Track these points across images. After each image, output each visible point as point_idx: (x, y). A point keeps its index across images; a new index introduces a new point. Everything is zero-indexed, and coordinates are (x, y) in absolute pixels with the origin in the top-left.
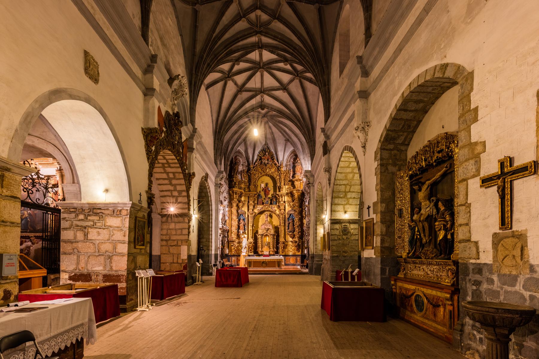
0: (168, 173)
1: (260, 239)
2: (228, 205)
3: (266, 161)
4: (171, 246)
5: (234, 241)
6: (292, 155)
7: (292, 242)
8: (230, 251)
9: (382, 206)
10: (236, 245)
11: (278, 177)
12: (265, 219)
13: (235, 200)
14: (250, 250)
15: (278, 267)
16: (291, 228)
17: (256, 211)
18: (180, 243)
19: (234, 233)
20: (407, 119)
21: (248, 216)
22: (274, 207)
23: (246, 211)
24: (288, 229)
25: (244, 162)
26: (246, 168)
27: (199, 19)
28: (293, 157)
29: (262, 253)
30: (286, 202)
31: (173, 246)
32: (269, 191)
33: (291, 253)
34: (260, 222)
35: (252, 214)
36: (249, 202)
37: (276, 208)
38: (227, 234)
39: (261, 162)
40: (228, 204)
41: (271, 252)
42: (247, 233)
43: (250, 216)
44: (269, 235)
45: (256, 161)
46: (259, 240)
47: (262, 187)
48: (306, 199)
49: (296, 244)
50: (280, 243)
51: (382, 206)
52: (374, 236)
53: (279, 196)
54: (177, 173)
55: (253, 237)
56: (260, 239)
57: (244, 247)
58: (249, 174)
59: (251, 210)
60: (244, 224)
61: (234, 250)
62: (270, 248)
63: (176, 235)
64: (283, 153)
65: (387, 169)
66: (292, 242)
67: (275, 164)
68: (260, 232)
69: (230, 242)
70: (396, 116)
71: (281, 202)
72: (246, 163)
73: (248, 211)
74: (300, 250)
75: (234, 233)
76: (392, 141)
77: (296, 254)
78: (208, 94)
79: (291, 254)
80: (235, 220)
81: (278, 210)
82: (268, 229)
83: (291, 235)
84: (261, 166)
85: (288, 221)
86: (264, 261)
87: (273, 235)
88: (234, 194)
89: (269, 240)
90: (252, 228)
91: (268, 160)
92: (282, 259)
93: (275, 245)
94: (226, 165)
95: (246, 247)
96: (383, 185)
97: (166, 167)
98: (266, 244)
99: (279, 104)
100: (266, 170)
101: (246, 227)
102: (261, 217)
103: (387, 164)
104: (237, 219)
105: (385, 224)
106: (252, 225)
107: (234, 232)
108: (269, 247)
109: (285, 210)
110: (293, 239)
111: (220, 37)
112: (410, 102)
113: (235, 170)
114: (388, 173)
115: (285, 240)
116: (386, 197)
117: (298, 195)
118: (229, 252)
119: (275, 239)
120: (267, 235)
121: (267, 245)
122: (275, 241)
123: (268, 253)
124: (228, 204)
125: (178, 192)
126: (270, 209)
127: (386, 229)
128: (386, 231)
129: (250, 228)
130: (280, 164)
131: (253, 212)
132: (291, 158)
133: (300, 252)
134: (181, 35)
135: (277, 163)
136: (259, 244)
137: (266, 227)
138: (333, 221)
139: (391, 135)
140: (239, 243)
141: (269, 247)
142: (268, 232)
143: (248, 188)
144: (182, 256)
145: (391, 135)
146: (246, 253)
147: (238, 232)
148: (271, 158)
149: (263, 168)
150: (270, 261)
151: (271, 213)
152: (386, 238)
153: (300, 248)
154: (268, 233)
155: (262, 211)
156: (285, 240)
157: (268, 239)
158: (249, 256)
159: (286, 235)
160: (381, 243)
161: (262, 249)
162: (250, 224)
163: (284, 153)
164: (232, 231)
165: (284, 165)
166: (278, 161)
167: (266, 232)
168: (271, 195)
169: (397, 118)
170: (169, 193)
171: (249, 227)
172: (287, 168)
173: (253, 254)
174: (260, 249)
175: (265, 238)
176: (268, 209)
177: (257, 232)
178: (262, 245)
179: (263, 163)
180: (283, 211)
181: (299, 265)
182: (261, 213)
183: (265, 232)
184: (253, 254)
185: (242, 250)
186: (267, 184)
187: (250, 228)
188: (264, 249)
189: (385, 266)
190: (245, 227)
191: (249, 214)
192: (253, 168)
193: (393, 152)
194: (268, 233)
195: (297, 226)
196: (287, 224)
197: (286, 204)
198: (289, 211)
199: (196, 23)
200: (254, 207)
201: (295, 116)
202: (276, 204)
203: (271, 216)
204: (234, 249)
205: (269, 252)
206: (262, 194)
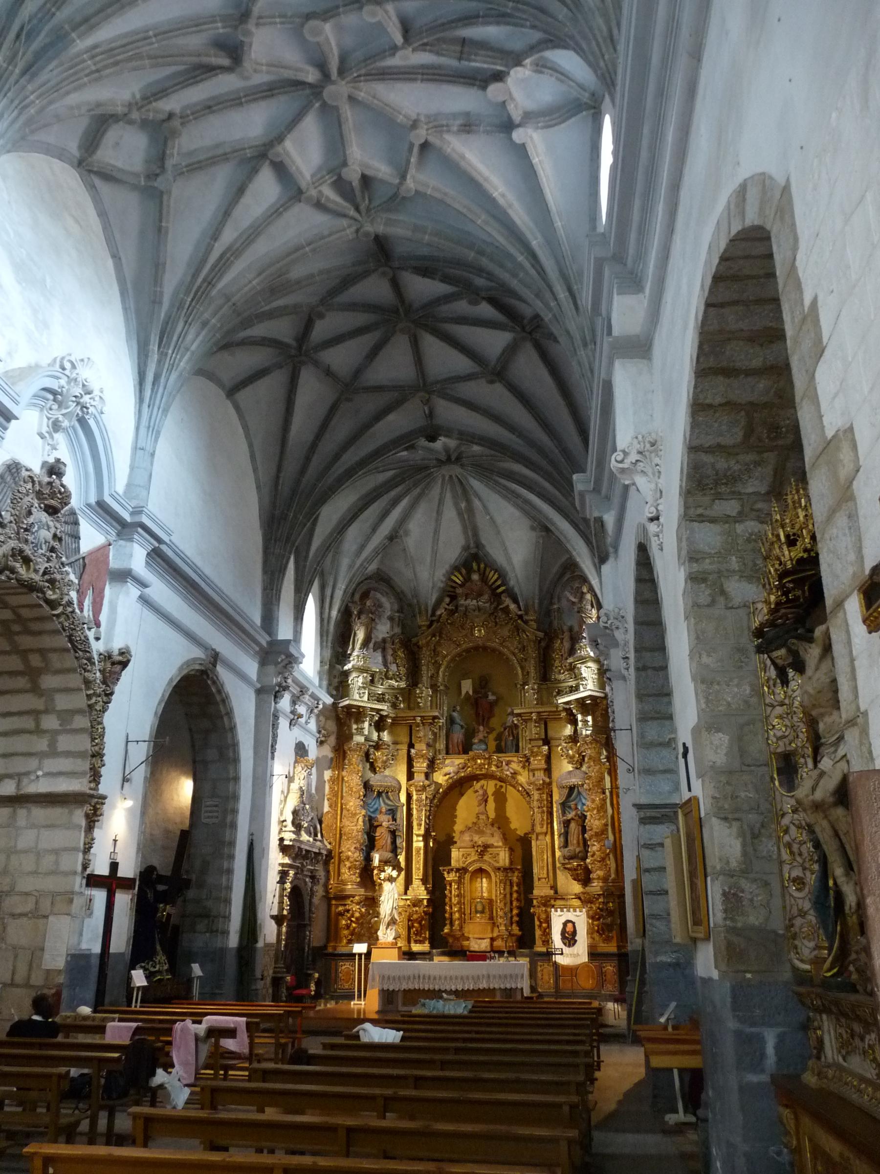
0: (24, 654)
1: (454, 886)
4: (13, 915)
5: (348, 897)
9: (716, 742)
10: (356, 909)
12: (477, 810)
16: (573, 839)
17: (440, 778)
18: (46, 905)
19: (348, 864)
20: (751, 404)
21: (409, 797)
23: (402, 778)
27: (168, 212)
31: (21, 915)
36: (411, 746)
37: (515, 766)
41: (499, 943)
42: (403, 864)
43: (415, 797)
46: (451, 892)
50: (535, 902)
51: (716, 742)
52: (706, 876)
54: (55, 650)
56: (454, 886)
57: (387, 919)
59: (419, 778)
60: (393, 828)
61: (346, 932)
63: (35, 873)
65: (723, 592)
70: (701, 396)
73: (410, 776)
76: (723, 489)
78: (237, 408)
82: (486, 847)
89: (490, 892)
93: (515, 912)
95: (392, 922)
96: (709, 656)
97: (18, 633)
98: (479, 908)
99: (533, 420)
101: (401, 843)
103: (719, 572)
105: (736, 824)
106: (422, 832)
107: (348, 858)
108: (491, 918)
111: (237, 249)
112: (729, 339)
114: (727, 608)
116: (729, 704)
120: (481, 871)
121: (482, 912)
122: (515, 895)
123: (483, 945)
125: (59, 718)
126: (494, 768)
127: (744, 845)
128: (745, 854)
134: (114, 256)
136: (453, 909)
137: (476, 838)
138: (650, 813)
139: (713, 465)
140: (372, 902)
141: (491, 918)
142: (485, 858)
144: (47, 956)
145: (713, 465)
147: (368, 859)
151: (499, 784)
152: (744, 883)
155: (461, 778)
156: (556, 892)
157: (484, 887)
158: (410, 955)
160: (725, 911)
164: (343, 856)
167: (476, 858)
169: (708, 401)
170: (28, 723)
171: (415, 838)
176: (484, 771)
177: (446, 859)
178: (461, 912)
182: (459, 785)
184: (425, 947)
189: (753, 1024)
190: (398, 841)
191: (413, 789)
192: (430, 626)
193: (739, 528)
199: (161, 221)
201: (541, 451)
203: (501, 799)
204: (348, 927)
205: (492, 940)
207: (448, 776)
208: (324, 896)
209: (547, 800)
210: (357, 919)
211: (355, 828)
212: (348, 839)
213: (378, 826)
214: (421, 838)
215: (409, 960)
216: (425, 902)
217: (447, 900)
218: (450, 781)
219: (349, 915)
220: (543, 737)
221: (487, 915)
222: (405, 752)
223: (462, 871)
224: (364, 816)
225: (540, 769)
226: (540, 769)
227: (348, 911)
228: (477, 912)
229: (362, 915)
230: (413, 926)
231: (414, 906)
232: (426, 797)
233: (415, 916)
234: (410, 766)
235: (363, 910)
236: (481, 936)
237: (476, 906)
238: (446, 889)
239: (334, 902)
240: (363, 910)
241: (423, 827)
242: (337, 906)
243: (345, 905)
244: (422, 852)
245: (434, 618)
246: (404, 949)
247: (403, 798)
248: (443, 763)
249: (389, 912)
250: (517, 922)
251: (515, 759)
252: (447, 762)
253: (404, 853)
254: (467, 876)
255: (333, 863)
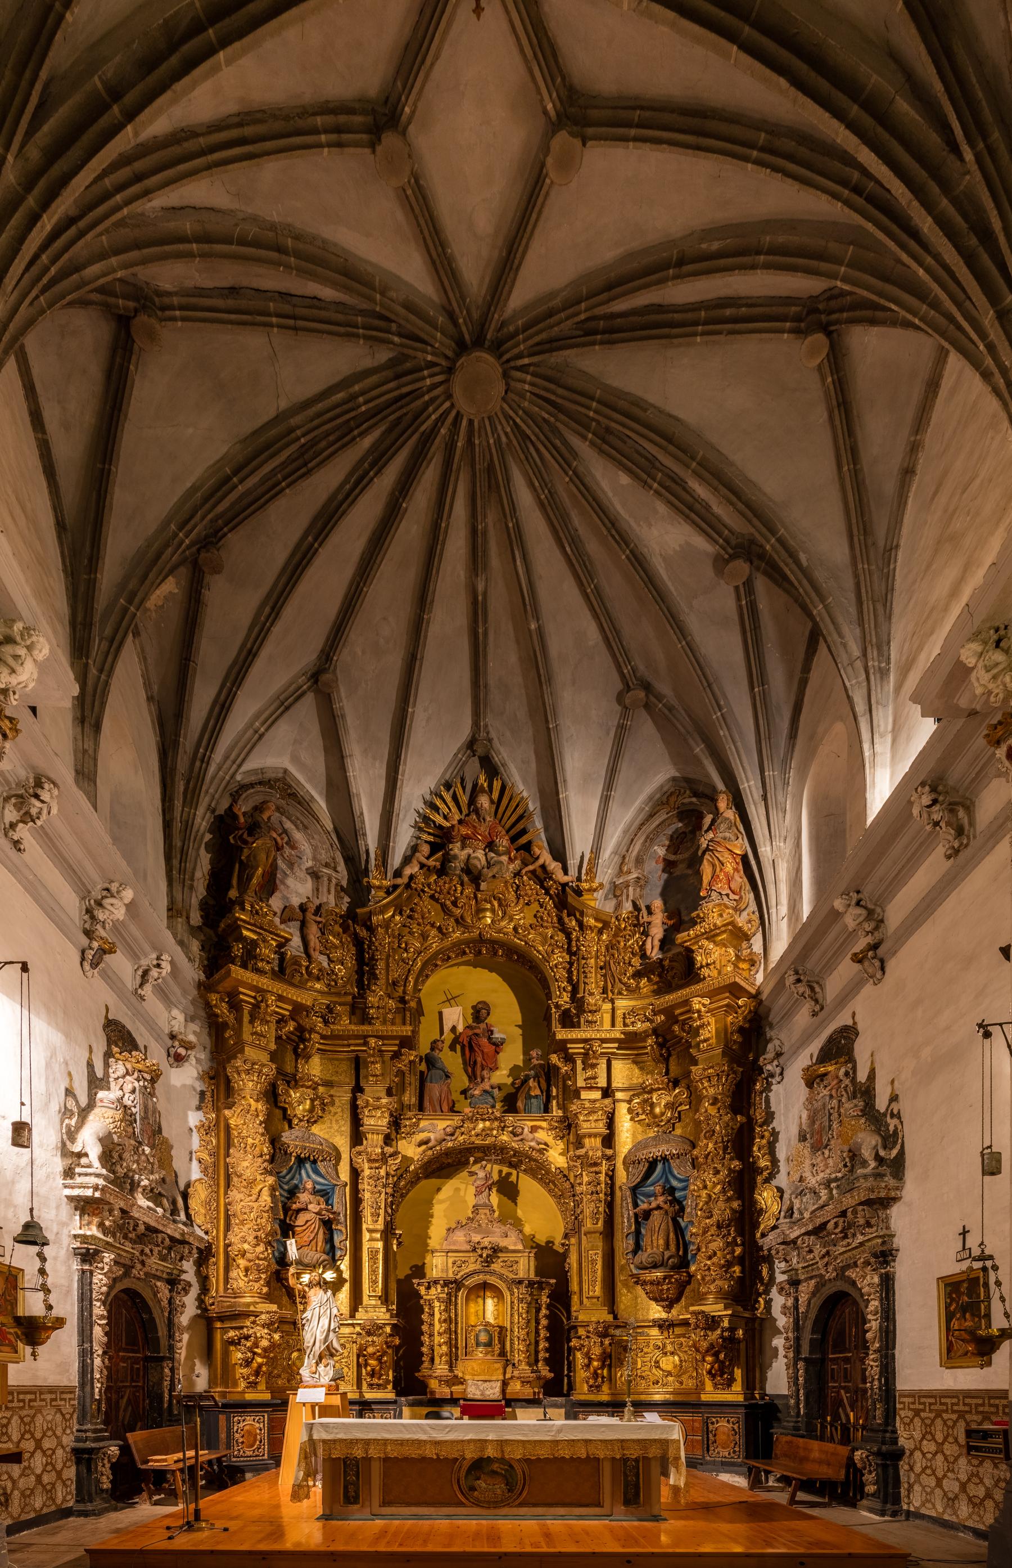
2: (202, 1094)
3: (480, 854)
5: (246, 1315)
6: (662, 816)
7: (663, 1325)
8: (223, 1374)
11: (559, 957)
13: (249, 1052)
14: (372, 1374)
15: (627, 1502)
17: (410, 1149)
21: (355, 1173)
22: (534, 1129)
23: (342, 1142)
24: (635, 1252)
25: (324, 856)
26: (338, 897)
28: (669, 831)
29: (457, 1389)
30: (619, 1095)
32: (498, 1046)
33: (657, 1389)
34: (434, 1221)
35: (384, 1158)
38: (198, 1273)
39: (447, 859)
40: (199, 1086)
41: (516, 1388)
44: (502, 1286)
45: (407, 860)
47: (447, 1028)
48: (779, 1055)
49: (714, 1335)
50: (581, 1332)
53: (569, 1059)
55: (394, 1297)
57: (319, 1348)
58: (363, 933)
59: (374, 1143)
60: (327, 1216)
61: (245, 1371)
62: (507, 1363)
64: (595, 805)
66: (663, 1325)
67: (542, 876)
68: (437, 1266)
69: (221, 1319)
71: (584, 1095)
72: (342, 867)
73: (357, 1137)
74: (738, 1373)
75: (242, 1262)
77: (704, 1398)
79: (657, 1398)
80: (251, 1183)
81: (561, 1145)
83: (658, 1283)
84: (444, 882)
85: (636, 1205)
86: (490, 1452)
87: (531, 1284)
88: (239, 1020)
90: (380, 1245)
91: (490, 846)
92: (665, 1443)
93: (543, 1345)
94: (177, 826)
95: (330, 1352)
98: (483, 1338)
100: (480, 911)
101: (342, 1239)
102: (442, 1195)
104: (271, 1180)
106: (380, 1225)
107: (243, 1254)
108: (503, 1353)
109: (609, 1140)
110: (669, 1308)
113: (247, 869)
115: (615, 1317)
117: (723, 1034)
118: (212, 1382)
119: (544, 1311)
120: (485, 1286)
122: (544, 1322)
123: (493, 1391)
124: (199, 1086)
129: (372, 1243)
130: (573, 872)
131: (389, 1150)
132: (650, 840)
133: (737, 1387)
135: (554, 866)
141: (503, 1353)
142: (496, 1267)
143: (353, 1013)
146: (330, 1391)
148: (513, 840)
149: (455, 904)
150: (544, 1453)
151: (506, 1170)
153: (734, 1361)
154: (493, 1273)
155: (448, 1153)
156: (615, 1317)
158: (364, 1408)
159: (621, 1290)
161: (451, 1367)
162: (372, 1224)
163: (606, 800)
164: (233, 1251)
165: (605, 874)
166: (559, 854)
167: (478, 1266)
168: (505, 1072)
171: (366, 1236)
172: (618, 906)
173: (391, 1396)
174: (441, 1368)
175: (473, 1308)
178: (452, 1345)
179: (457, 865)
180: (593, 1146)
181: (727, 1466)
183: (472, 1267)
185: (305, 1372)
186: (480, 1012)
187: (372, 1243)
188: (464, 1368)
190: (337, 1239)
194: (493, 1273)
195: (719, 1226)
196: (624, 1221)
197: (622, 1109)
198: (638, 1146)
200: (396, 1123)
202: (547, 1109)
203: (509, 1190)
204: (248, 1363)
205: (505, 1384)
206: (452, 1061)
207: (424, 1147)
208: (197, 1316)
209: (606, 1184)
210: (265, 1350)
211: (255, 1205)
212: (242, 1222)
213: (299, 1211)
214: (378, 1236)
215: (360, 1415)
216: (388, 1329)
217: (425, 1328)
218: (430, 1153)
219: (249, 1344)
220: (605, 1085)
221: (497, 1348)
222: (347, 1097)
223: (454, 1285)
224: (273, 1189)
225: (595, 1135)
226: (595, 1135)
227: (247, 1338)
228: (478, 1344)
229: (273, 1345)
230: (366, 1365)
231: (369, 1333)
232: (388, 1174)
233: (370, 1350)
234: (356, 1122)
235: (276, 1336)
236: (487, 1378)
237: (477, 1336)
238: (423, 1312)
239: (218, 1325)
240: (276, 1336)
241: (381, 1219)
242: (225, 1330)
243: (242, 1328)
244: (380, 1256)
245: (399, 881)
246: (350, 1396)
247: (345, 1175)
248: (416, 1124)
249: (320, 1337)
250: (545, 1360)
251: (544, 1124)
252: (423, 1124)
253: (347, 1258)
254: (462, 1294)
255: (215, 1264)
